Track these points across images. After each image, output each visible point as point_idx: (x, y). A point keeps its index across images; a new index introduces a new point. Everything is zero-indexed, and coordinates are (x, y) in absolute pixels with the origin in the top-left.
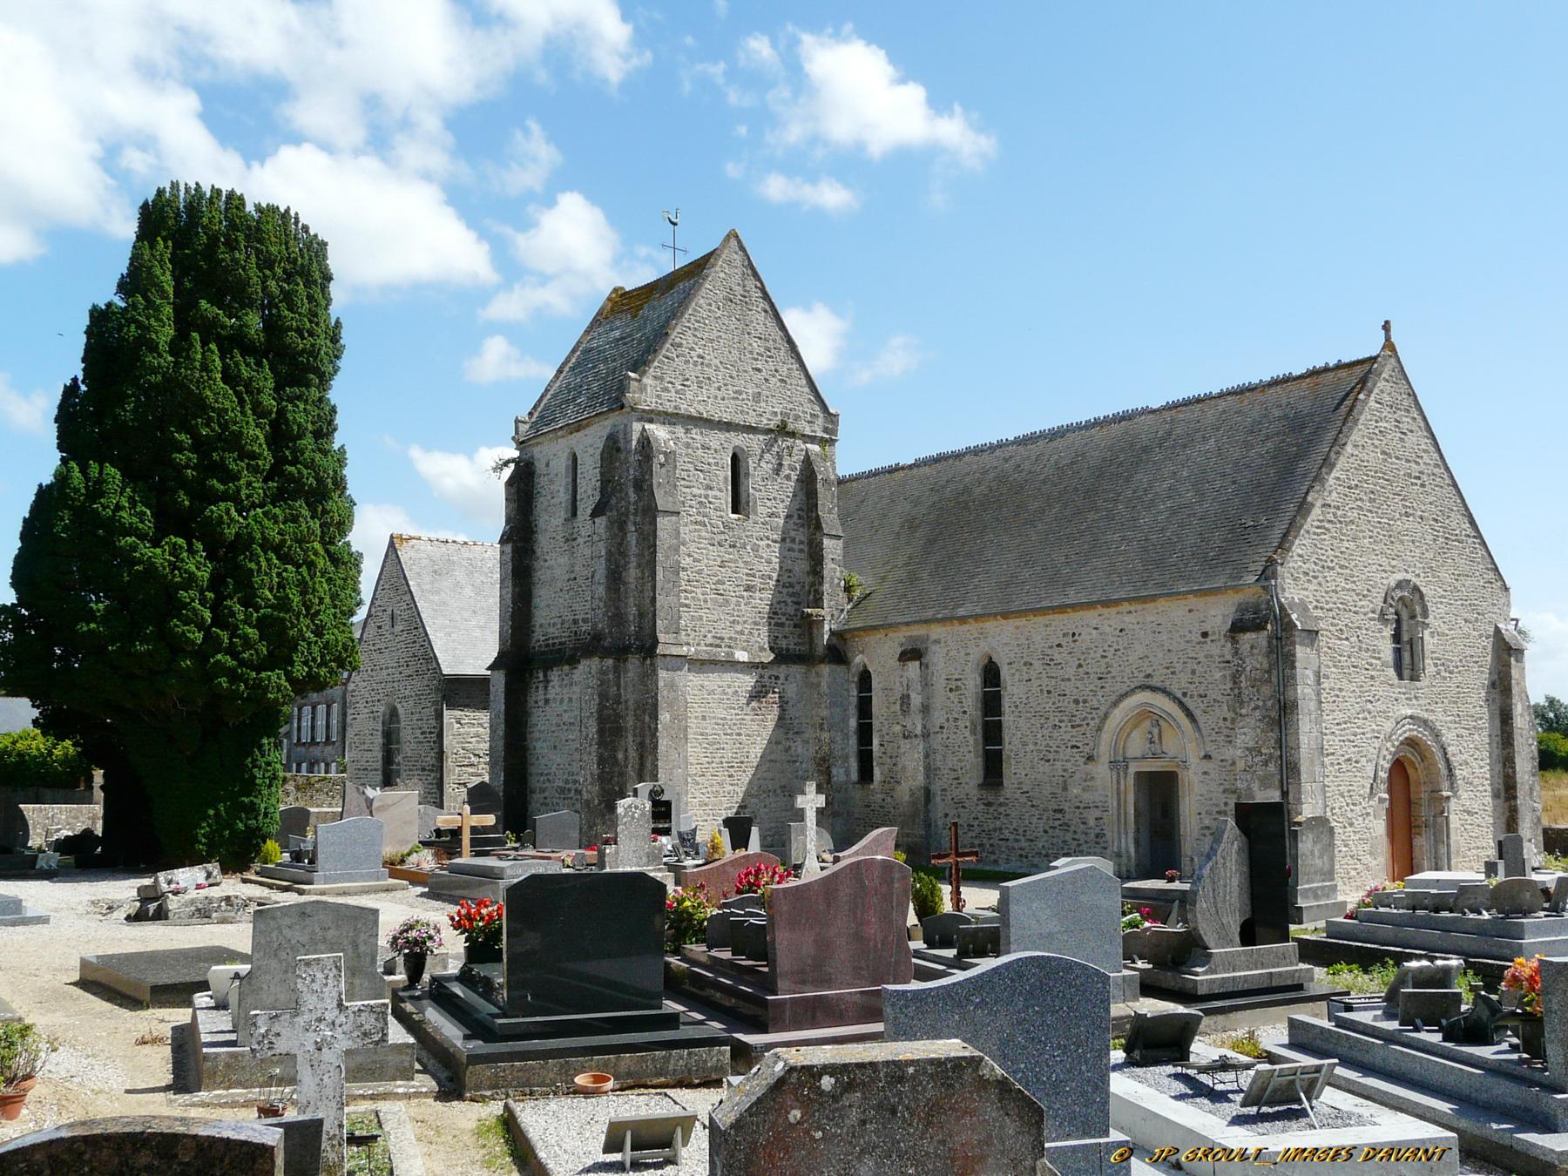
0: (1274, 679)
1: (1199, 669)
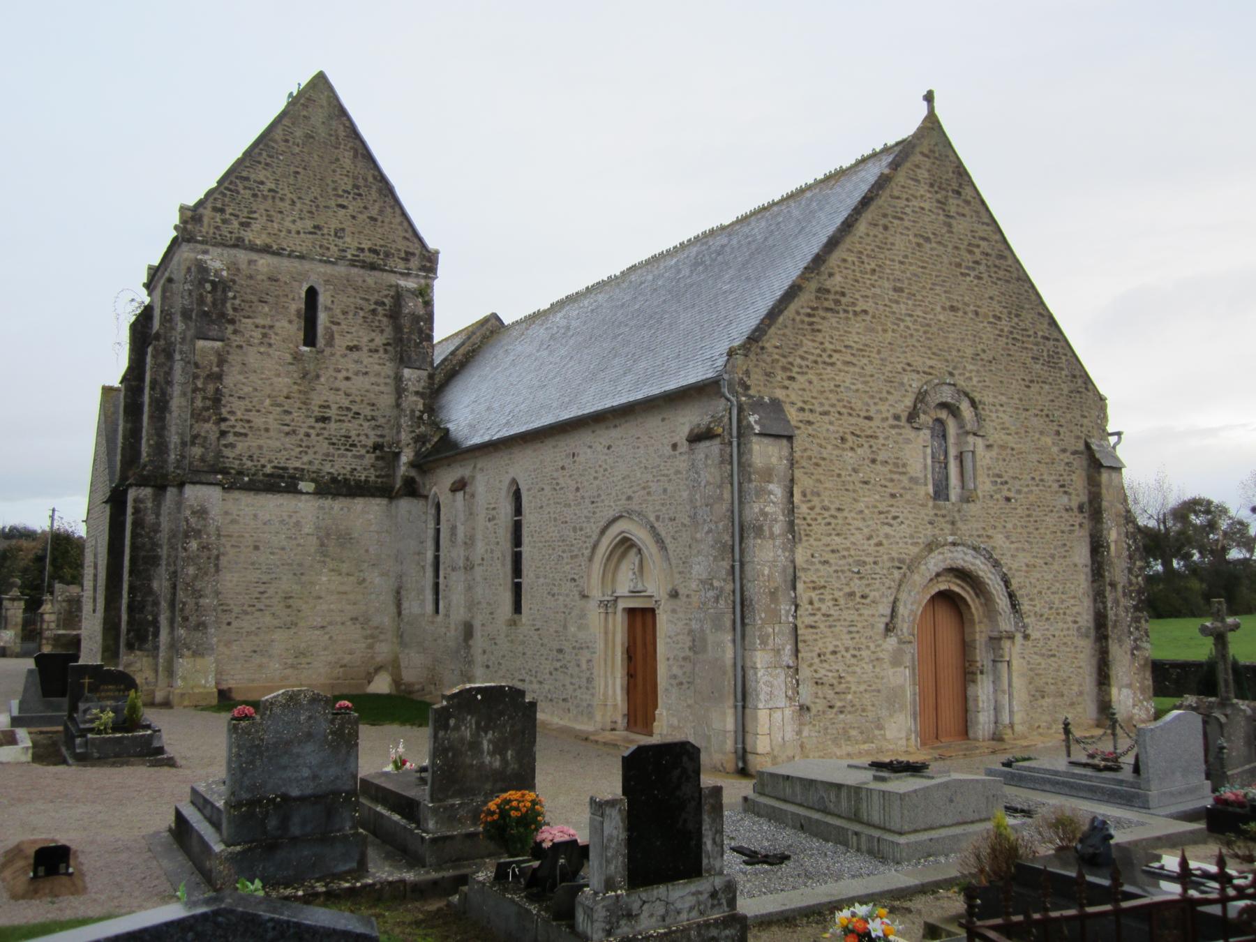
0: (727, 495)
1: (670, 488)
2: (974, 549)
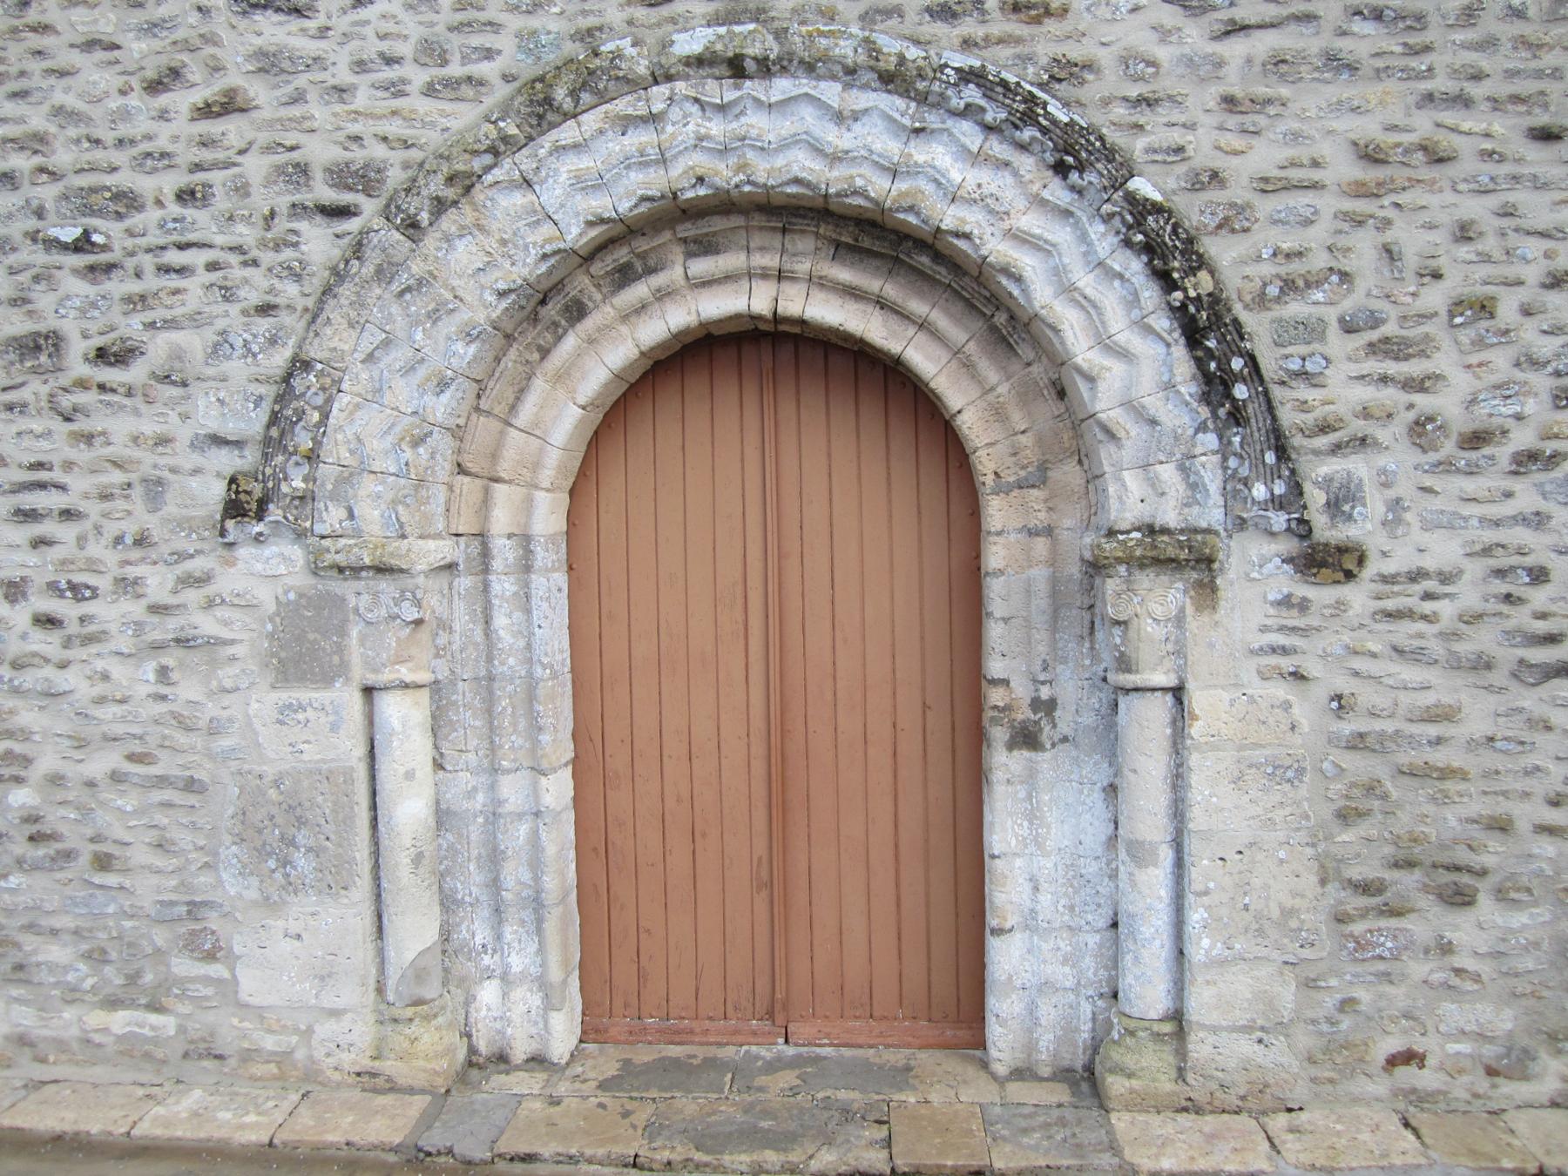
2: (892, 79)
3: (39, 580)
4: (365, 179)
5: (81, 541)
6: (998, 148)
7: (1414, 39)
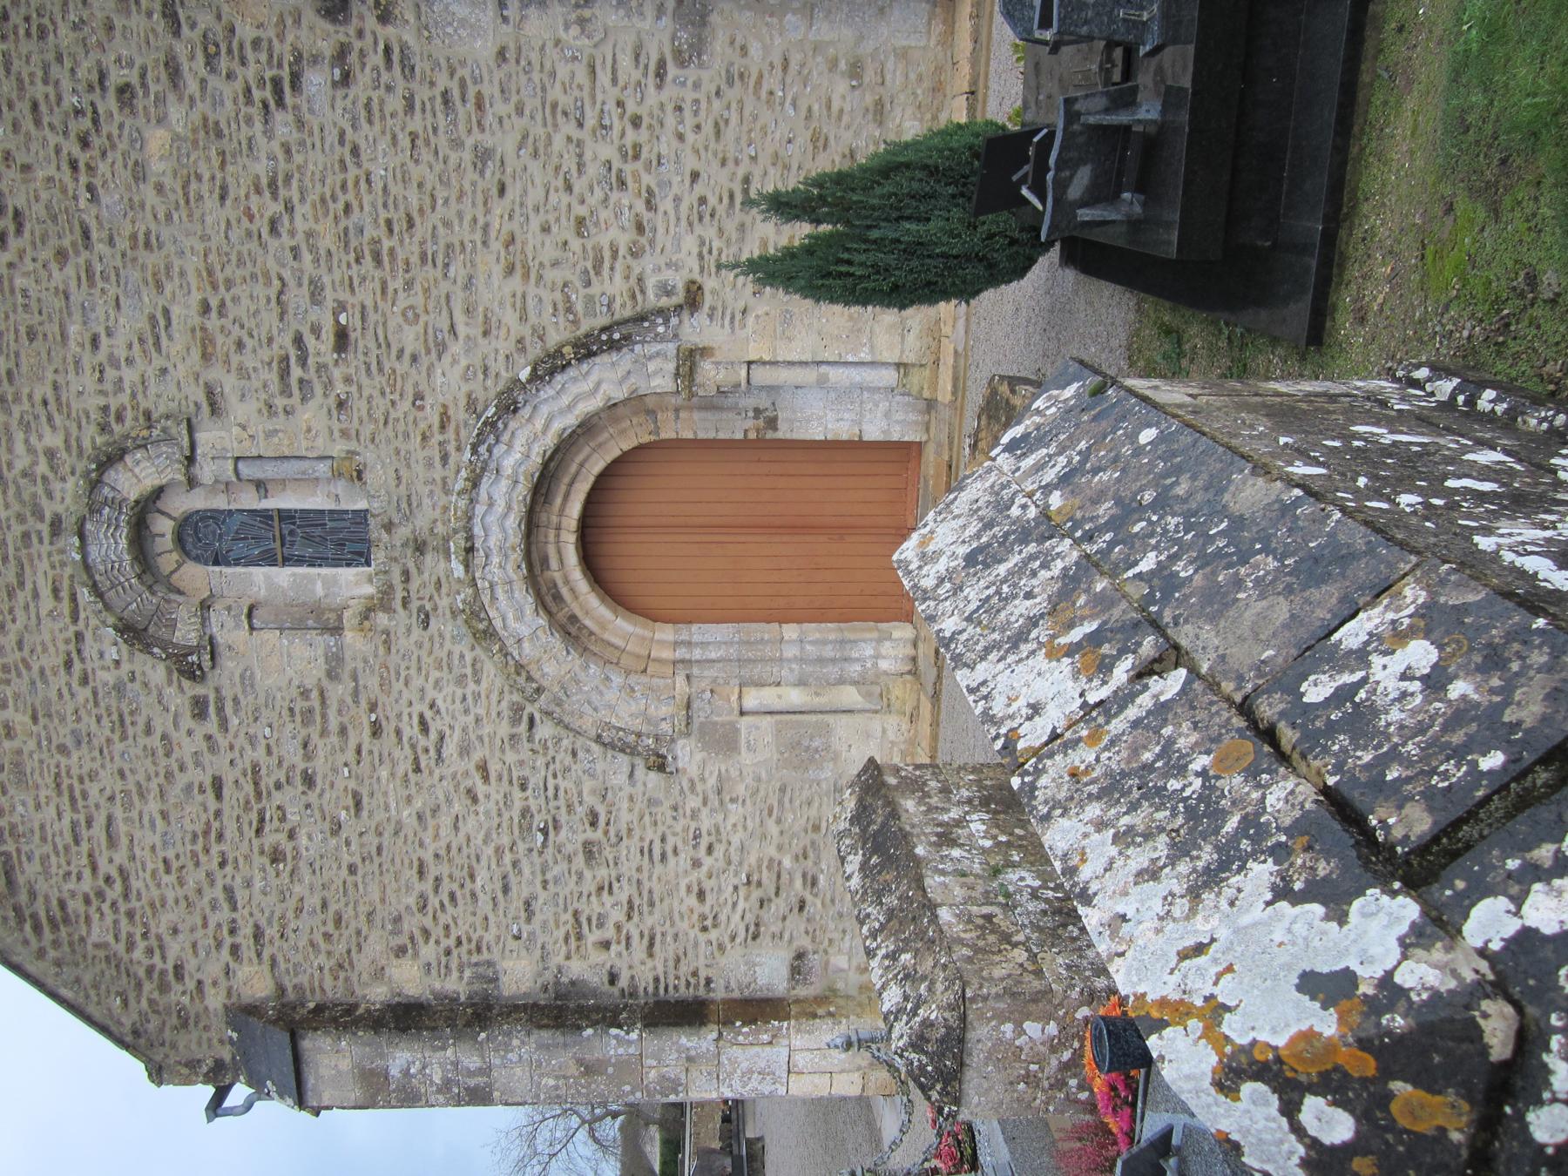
2: (475, 483)
3: (692, 852)
4: (517, 710)
5: (675, 834)
6: (505, 437)
7: (458, 249)
